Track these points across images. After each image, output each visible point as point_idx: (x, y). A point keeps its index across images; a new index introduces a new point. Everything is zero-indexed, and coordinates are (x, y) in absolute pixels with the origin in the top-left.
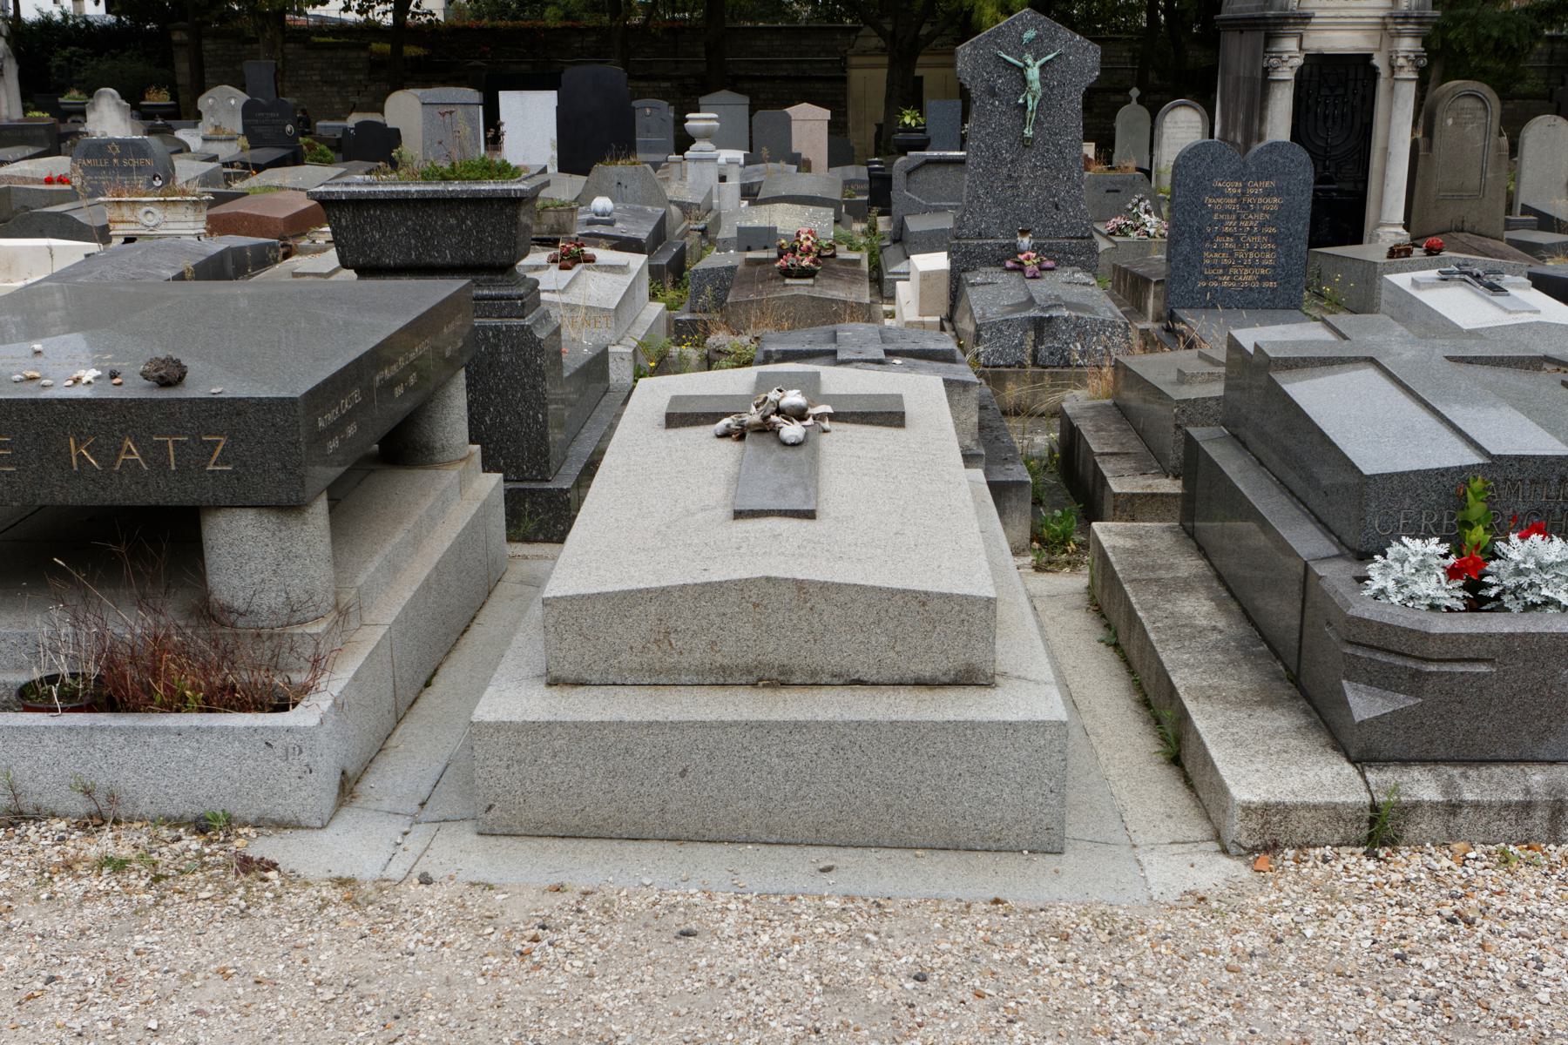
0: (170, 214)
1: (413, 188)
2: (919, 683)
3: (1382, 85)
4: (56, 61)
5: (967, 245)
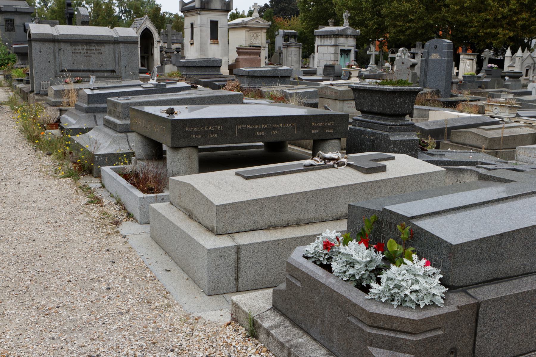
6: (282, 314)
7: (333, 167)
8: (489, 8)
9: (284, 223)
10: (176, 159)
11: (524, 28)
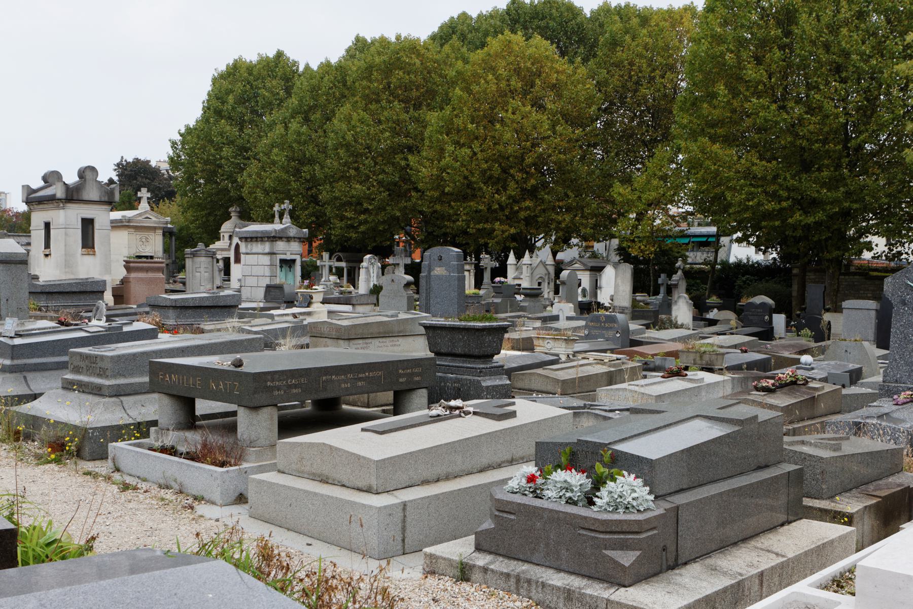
0: (557, 344)
4: (739, 282)
5: (888, 386)
6: (490, 553)
7: (460, 416)
8: (479, 194)
9: (435, 478)
10: (255, 422)
11: (528, 221)
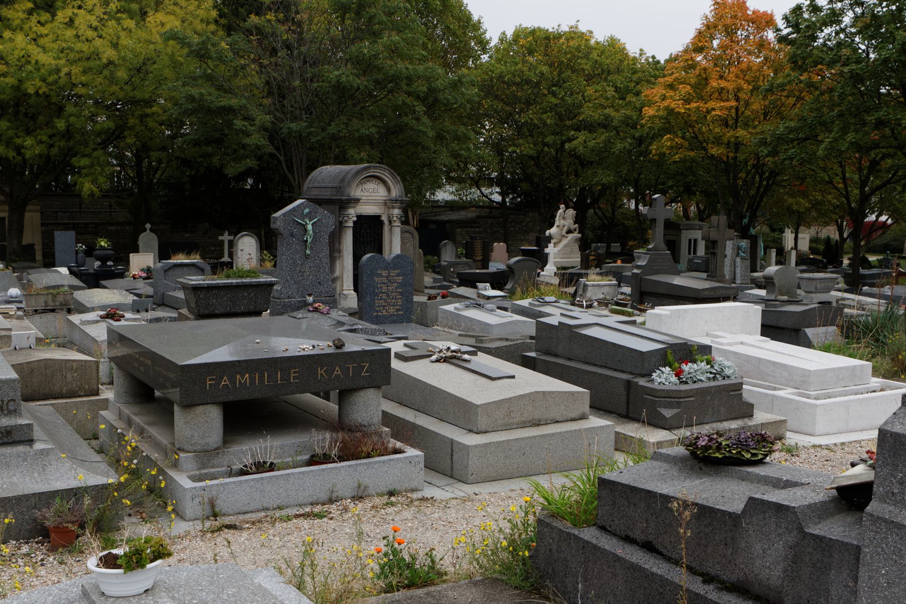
1: (234, 281)
2: (572, 420)
3: (386, 228)
